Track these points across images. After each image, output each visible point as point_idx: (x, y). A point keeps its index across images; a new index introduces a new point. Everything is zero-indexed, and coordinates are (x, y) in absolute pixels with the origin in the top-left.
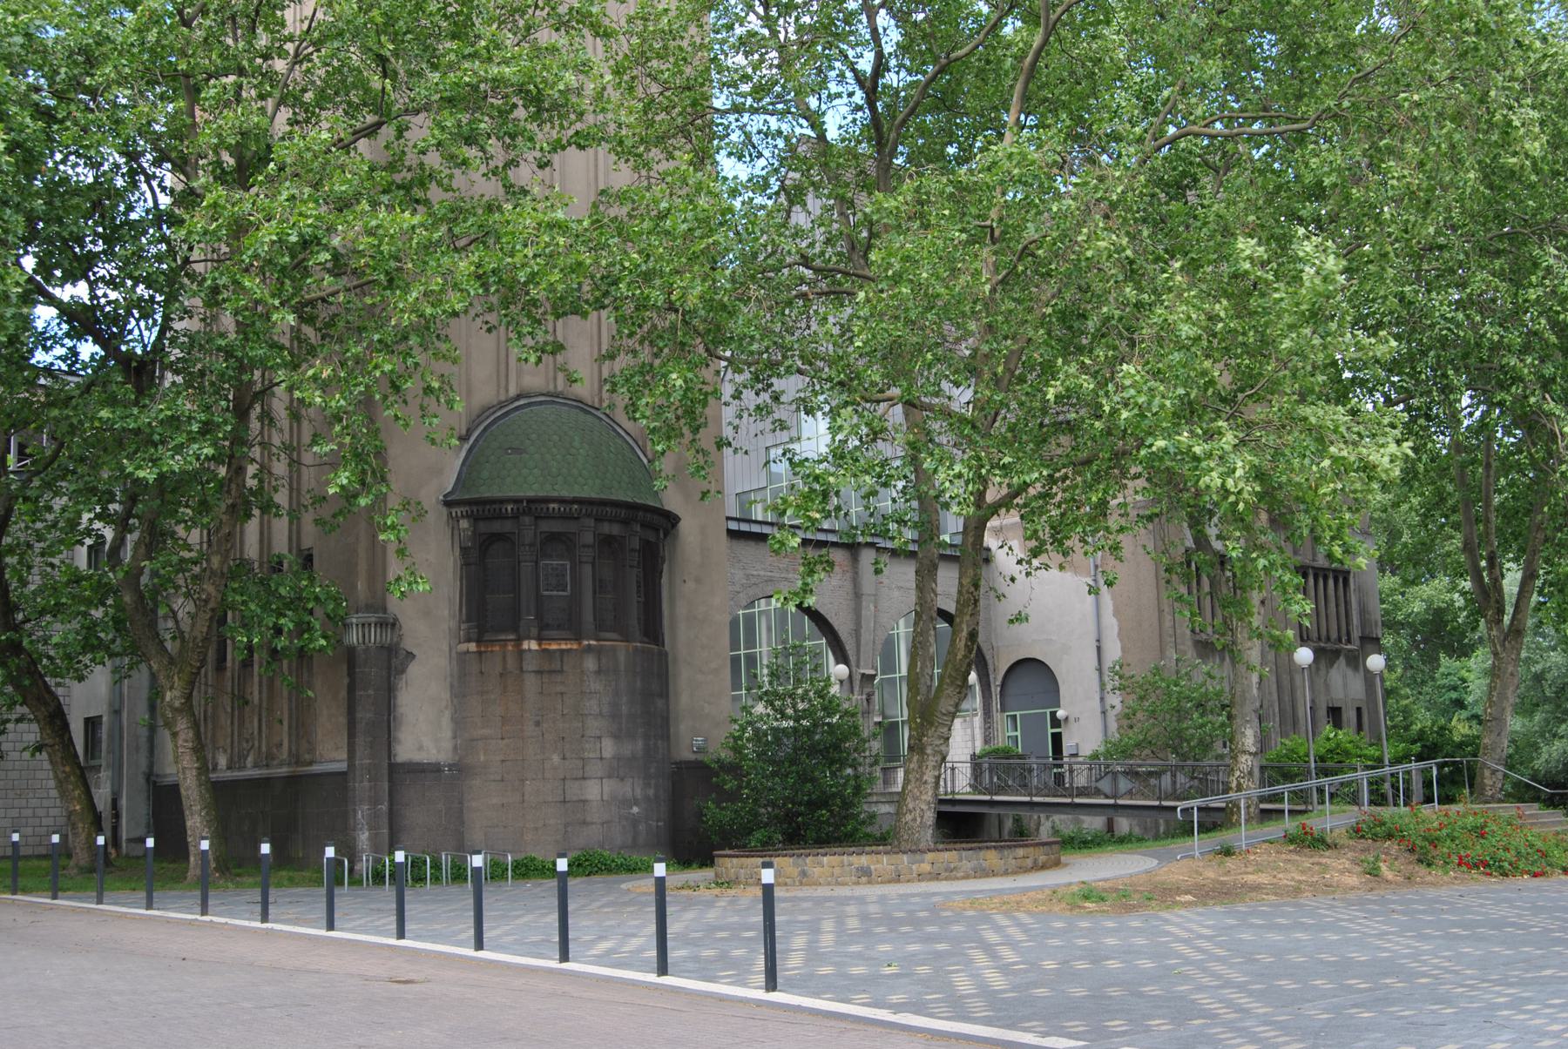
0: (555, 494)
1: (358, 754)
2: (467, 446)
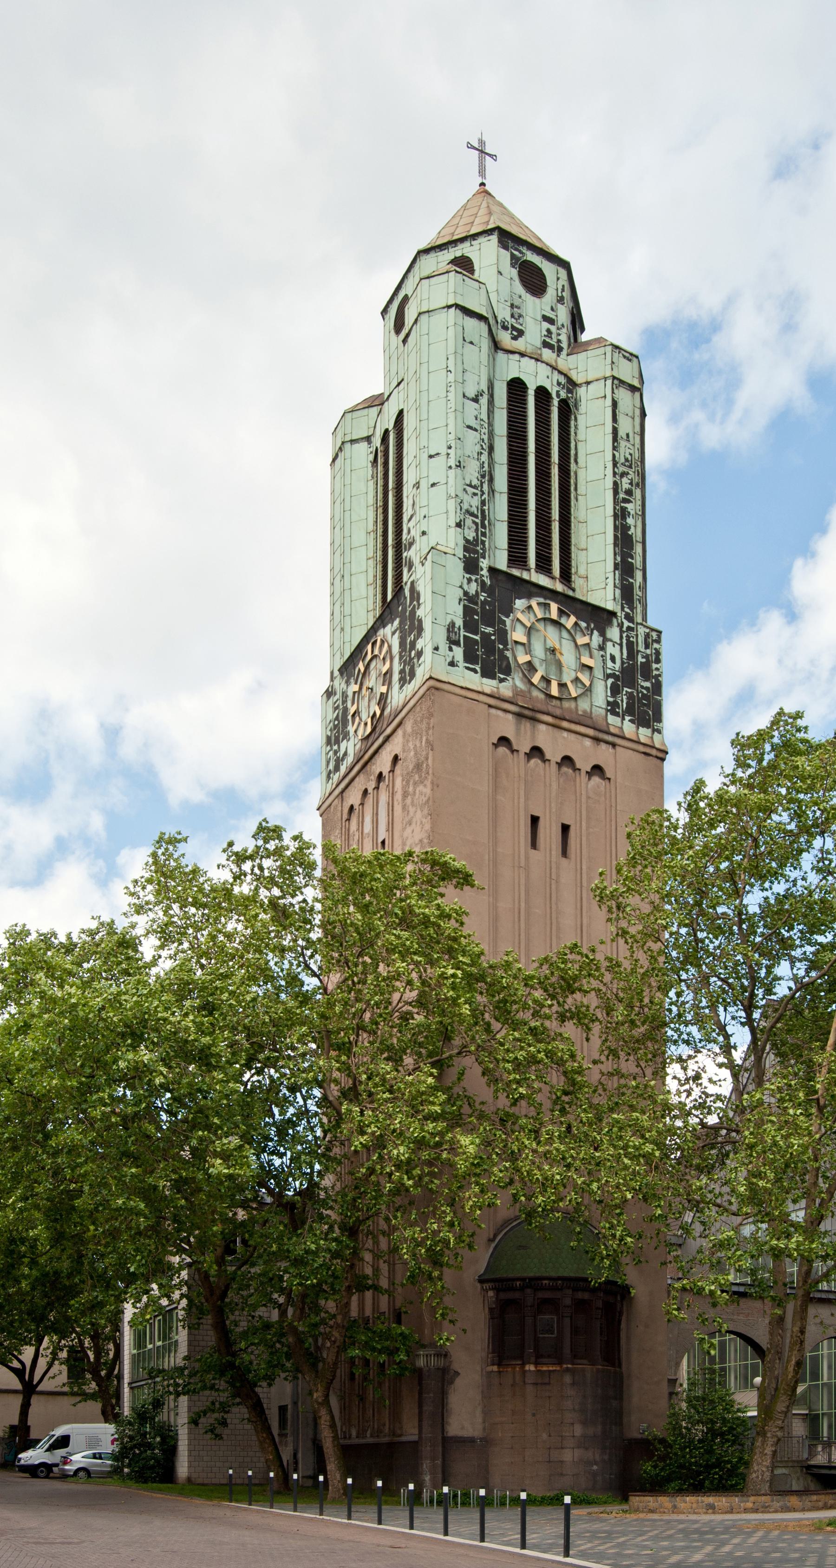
0: (519, 1275)
1: (424, 1430)
2: (493, 1245)
